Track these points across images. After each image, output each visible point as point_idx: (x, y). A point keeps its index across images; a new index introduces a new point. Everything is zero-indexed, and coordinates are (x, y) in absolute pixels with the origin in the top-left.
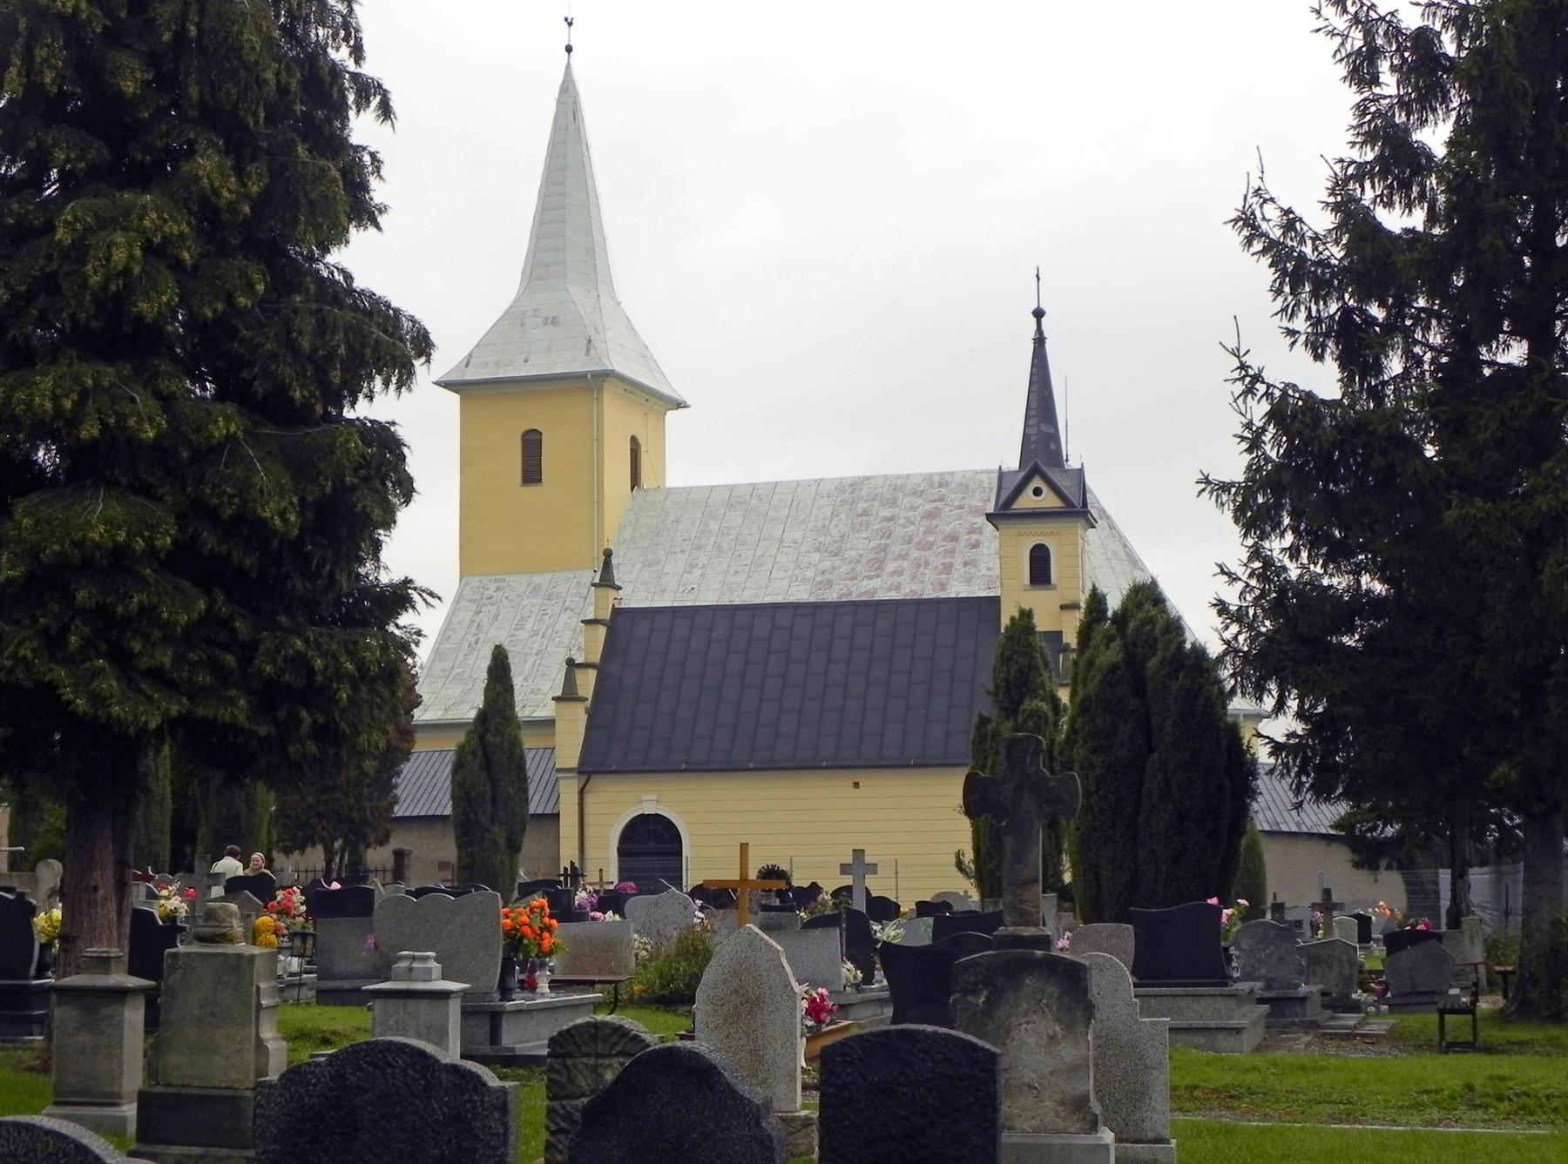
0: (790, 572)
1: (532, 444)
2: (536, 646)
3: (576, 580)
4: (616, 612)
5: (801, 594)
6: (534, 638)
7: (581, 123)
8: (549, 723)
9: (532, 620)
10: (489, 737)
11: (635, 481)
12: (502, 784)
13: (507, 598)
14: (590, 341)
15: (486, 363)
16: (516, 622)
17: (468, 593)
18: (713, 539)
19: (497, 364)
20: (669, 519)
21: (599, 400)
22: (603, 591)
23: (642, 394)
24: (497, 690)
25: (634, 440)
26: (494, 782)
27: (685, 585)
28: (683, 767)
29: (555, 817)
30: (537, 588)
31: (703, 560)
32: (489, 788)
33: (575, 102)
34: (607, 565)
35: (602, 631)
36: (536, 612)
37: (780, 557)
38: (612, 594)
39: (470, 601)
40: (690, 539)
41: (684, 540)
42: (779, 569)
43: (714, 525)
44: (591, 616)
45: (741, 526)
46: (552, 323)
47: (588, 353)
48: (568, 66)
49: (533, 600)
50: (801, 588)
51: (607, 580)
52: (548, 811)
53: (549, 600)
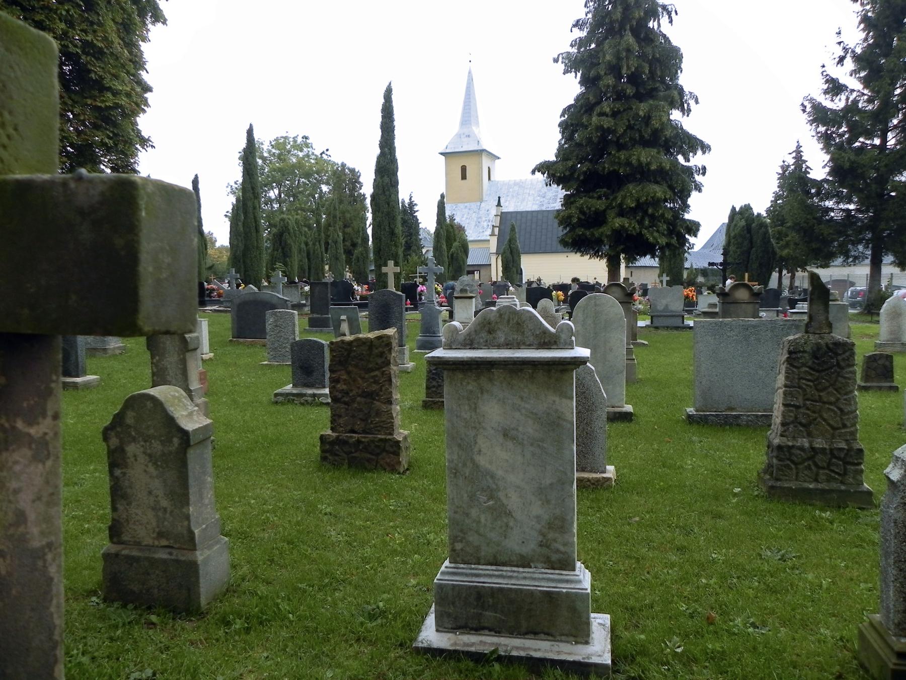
1: (464, 169)
4: (502, 213)
5: (535, 208)
8: (489, 241)
11: (489, 179)
26: (513, 256)
30: (466, 207)
43: (511, 190)
51: (499, 205)
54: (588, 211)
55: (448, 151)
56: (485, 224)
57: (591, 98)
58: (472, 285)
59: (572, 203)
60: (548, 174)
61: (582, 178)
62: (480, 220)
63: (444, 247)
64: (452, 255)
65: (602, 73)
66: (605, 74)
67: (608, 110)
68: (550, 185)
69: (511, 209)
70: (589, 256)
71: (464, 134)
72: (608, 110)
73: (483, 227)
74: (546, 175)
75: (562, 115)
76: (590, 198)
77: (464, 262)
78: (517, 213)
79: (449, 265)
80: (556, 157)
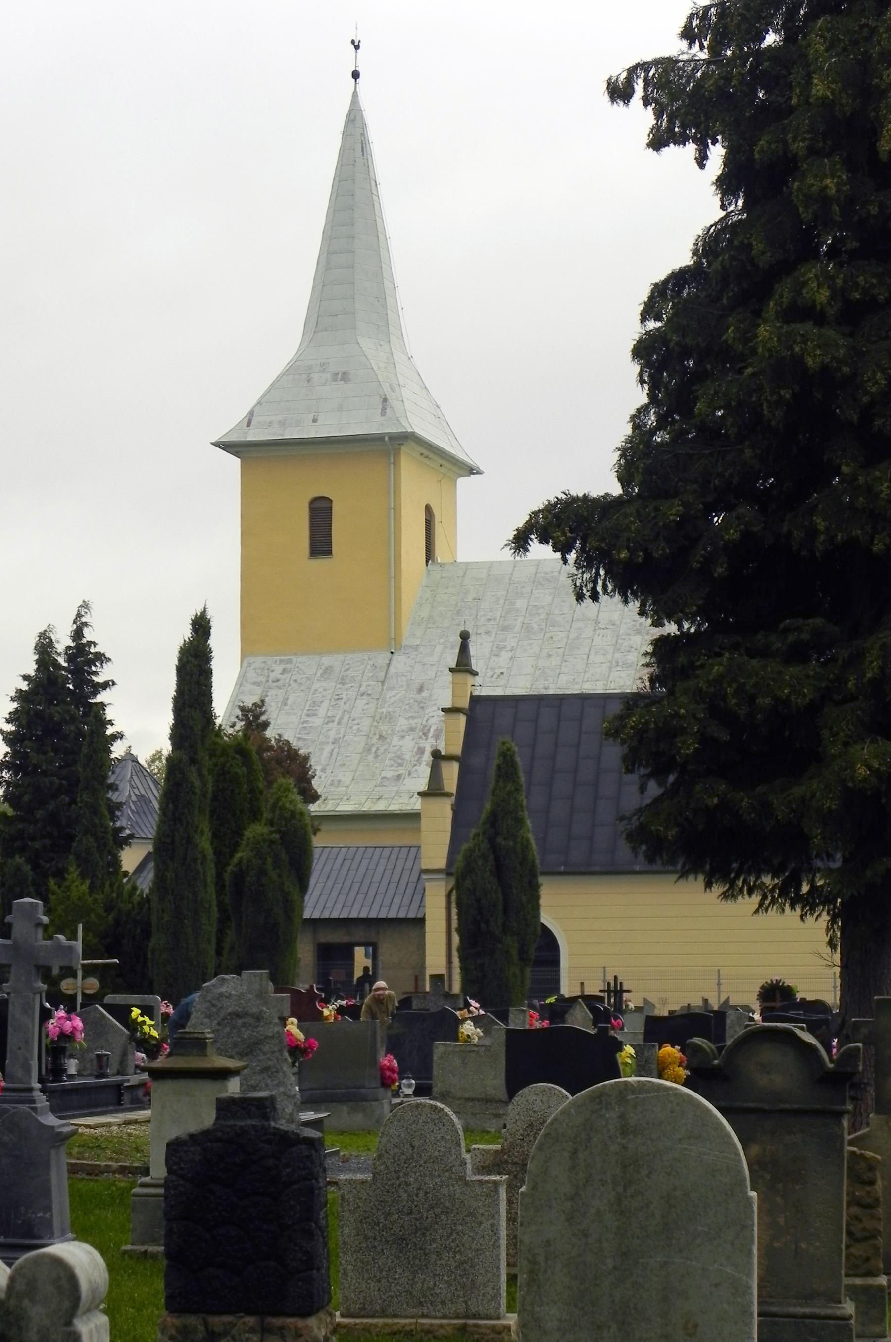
0: (609, 657)
2: (332, 734)
3: (371, 663)
4: (475, 700)
6: (330, 725)
7: (369, 158)
8: (414, 817)
9: (325, 705)
10: (499, 840)
12: (514, 890)
13: (295, 681)
14: (385, 400)
15: (270, 423)
16: (307, 707)
17: (251, 675)
18: (520, 619)
19: (283, 423)
20: (470, 597)
21: (396, 464)
22: (461, 677)
23: (436, 458)
24: (508, 788)
25: (428, 509)
27: (492, 669)
28: (562, 869)
29: (420, 922)
30: (328, 671)
31: (511, 642)
32: (500, 895)
33: (363, 134)
34: (464, 649)
35: (462, 719)
36: (329, 697)
37: (597, 640)
38: (470, 679)
39: (254, 683)
40: (495, 619)
41: (489, 620)
42: (597, 653)
43: (521, 604)
44: (448, 705)
45: (551, 605)
46: (343, 379)
47: (383, 412)
48: (355, 94)
49: (324, 684)
50: (623, 674)
52: (412, 915)
53: (343, 684)
54: (742, 712)
55: (254, 435)
56: (408, 745)
57: (758, 246)
58: (258, 1018)
59: (685, 673)
60: (582, 550)
61: (720, 571)
62: (384, 728)
63: (205, 843)
64: (239, 876)
65: (799, 146)
66: (813, 151)
67: (823, 296)
68: (595, 597)
69: (519, 686)
70: (756, 899)
71: (323, 367)
72: (823, 296)
73: (399, 759)
74: (572, 556)
75: (649, 311)
76: (752, 654)
77: (291, 907)
78: (539, 701)
79: (224, 921)
80: (624, 478)
